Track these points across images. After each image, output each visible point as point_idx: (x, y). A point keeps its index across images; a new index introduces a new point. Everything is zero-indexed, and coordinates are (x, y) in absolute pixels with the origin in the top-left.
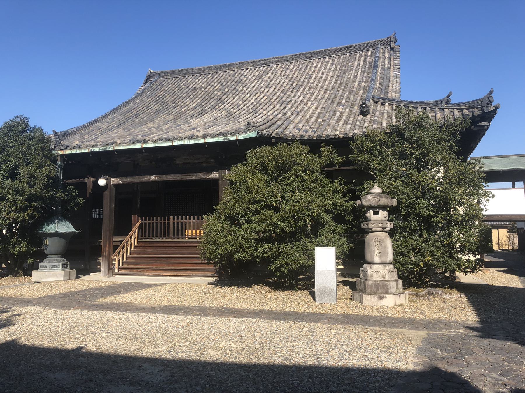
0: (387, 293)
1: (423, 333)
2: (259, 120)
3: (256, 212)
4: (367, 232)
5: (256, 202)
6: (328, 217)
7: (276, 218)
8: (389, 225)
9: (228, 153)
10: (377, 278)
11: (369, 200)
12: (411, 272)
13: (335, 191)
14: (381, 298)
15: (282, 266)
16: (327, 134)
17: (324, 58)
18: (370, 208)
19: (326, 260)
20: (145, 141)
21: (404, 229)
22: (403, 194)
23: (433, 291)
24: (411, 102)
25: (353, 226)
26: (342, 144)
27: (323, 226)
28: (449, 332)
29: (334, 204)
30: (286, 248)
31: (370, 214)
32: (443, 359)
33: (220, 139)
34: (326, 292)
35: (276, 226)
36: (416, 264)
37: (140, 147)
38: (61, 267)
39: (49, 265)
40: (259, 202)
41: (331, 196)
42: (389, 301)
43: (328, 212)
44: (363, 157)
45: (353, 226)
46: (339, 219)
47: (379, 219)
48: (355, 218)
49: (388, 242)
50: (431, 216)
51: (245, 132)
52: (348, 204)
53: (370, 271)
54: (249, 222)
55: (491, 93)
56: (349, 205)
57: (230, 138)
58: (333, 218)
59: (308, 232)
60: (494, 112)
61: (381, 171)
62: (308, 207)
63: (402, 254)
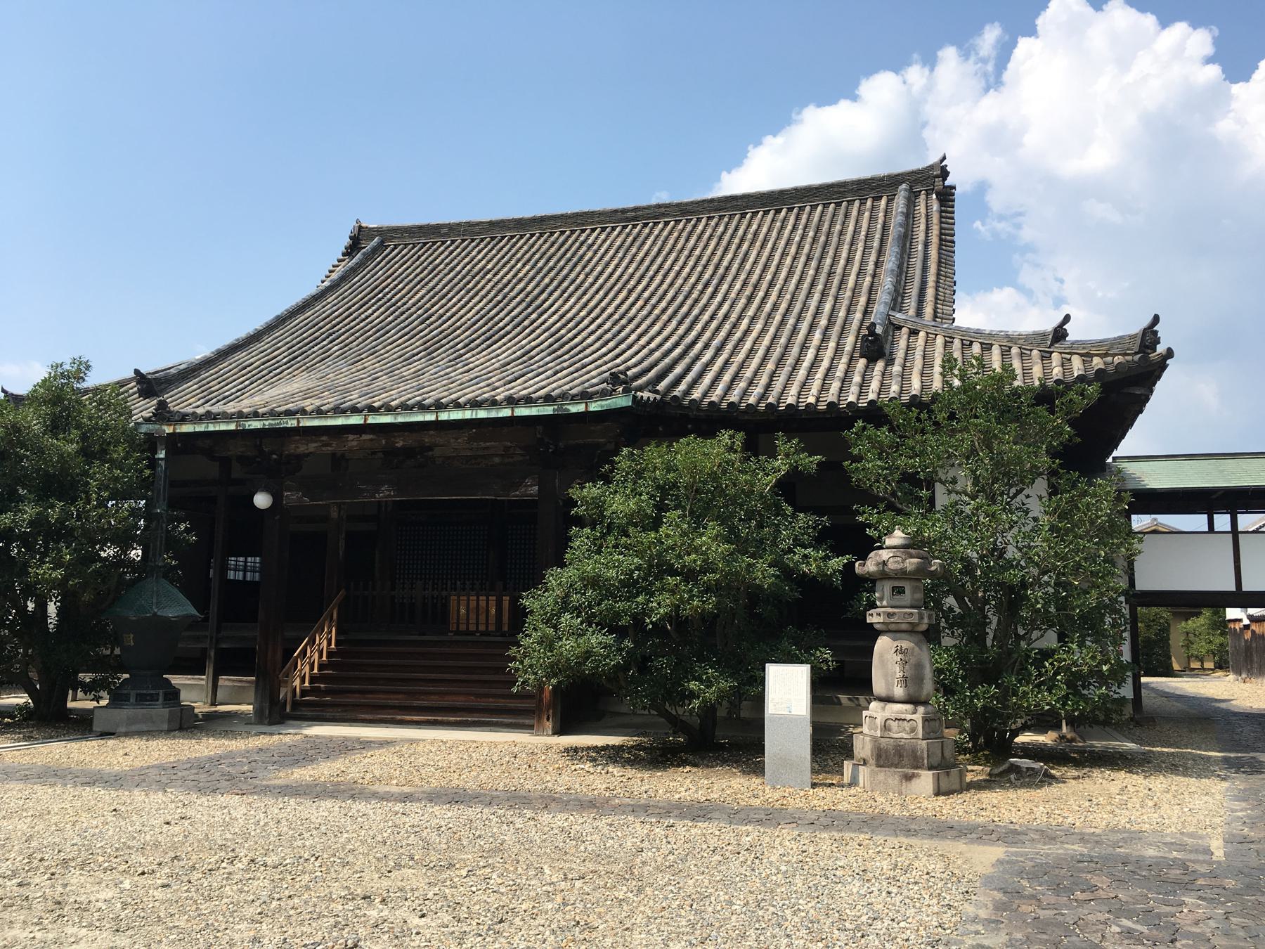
1: (996, 852)
2: (630, 362)
9: (566, 445)
16: (788, 402)
17: (778, 211)
19: (788, 689)
20: (372, 409)
24: (978, 332)
26: (823, 425)
28: (1055, 850)
32: (1033, 897)
33: (548, 410)
37: (362, 422)
38: (161, 699)
39: (133, 693)
51: (604, 394)
55: (1156, 319)
57: (569, 407)
60: (1161, 366)
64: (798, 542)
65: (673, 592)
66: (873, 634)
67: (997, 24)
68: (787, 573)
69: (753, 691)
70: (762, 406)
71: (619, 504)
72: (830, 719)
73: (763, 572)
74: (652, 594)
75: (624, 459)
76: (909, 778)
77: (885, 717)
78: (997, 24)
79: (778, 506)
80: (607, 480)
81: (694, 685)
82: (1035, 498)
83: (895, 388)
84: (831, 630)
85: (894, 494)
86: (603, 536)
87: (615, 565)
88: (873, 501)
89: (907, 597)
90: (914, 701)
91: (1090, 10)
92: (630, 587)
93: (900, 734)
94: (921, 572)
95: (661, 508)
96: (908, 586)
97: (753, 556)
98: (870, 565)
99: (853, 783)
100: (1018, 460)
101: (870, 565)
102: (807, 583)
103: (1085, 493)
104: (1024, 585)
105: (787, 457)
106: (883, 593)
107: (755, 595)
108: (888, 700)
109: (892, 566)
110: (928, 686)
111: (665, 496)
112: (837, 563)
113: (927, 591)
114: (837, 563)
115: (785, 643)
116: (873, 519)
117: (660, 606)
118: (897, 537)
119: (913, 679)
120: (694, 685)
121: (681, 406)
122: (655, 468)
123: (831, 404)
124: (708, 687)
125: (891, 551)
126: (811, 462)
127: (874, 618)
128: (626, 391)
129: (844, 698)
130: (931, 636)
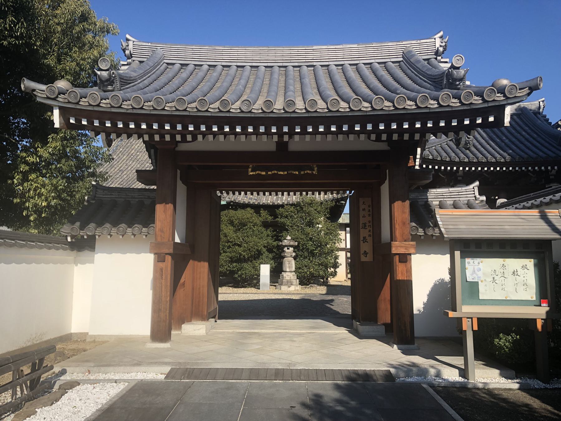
0: (292, 285)
3: (229, 247)
4: (284, 257)
5: (230, 242)
6: (264, 250)
7: (240, 250)
8: (294, 254)
10: (288, 278)
11: (285, 242)
12: (304, 278)
13: (268, 236)
14: (289, 287)
15: (242, 274)
18: (286, 246)
21: (301, 256)
22: (301, 239)
23: (313, 285)
25: (277, 254)
27: (262, 254)
29: (268, 243)
30: (245, 265)
31: (286, 249)
34: (265, 285)
35: (241, 255)
36: (306, 273)
40: (231, 242)
41: (264, 239)
42: (292, 288)
43: (265, 247)
44: (283, 220)
45: (277, 254)
46: (270, 251)
47: (289, 251)
48: (278, 250)
49: (293, 262)
50: (314, 250)
52: (275, 243)
53: (284, 275)
54: (224, 252)
56: (275, 243)
58: (267, 250)
59: (257, 256)
61: (292, 227)
62: (257, 246)
63: (300, 268)
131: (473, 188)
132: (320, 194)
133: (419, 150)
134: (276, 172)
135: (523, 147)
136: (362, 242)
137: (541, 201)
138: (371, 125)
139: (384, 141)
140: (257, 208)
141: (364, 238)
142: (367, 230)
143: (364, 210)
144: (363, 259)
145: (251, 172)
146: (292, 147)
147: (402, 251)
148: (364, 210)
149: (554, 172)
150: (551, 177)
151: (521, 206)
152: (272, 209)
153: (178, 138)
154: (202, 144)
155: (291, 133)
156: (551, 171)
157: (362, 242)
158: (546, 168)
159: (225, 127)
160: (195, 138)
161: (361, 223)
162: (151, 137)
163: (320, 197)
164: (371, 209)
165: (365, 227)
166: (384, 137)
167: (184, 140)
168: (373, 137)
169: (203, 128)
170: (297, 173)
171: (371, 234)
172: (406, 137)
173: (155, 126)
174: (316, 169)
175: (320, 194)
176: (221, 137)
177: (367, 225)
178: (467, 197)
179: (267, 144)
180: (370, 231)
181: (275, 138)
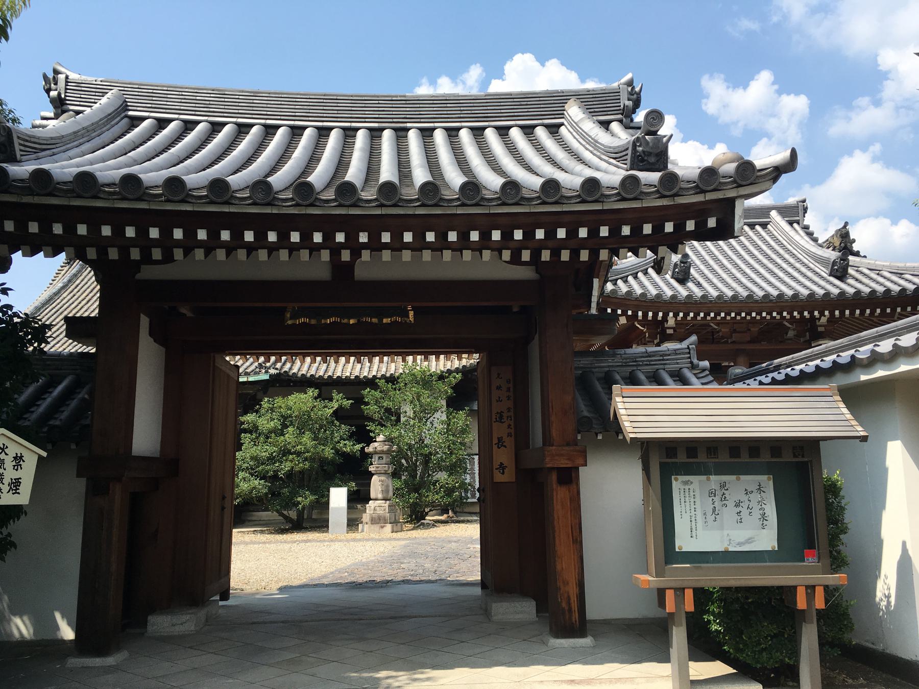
19: (338, 497)
51: (256, 373)
64: (342, 438)
65: (291, 461)
66: (371, 475)
67: (478, 65)
68: (337, 452)
69: (324, 500)
70: (326, 377)
71: (266, 423)
72: (354, 516)
73: (328, 452)
74: (282, 462)
75: (265, 403)
76: (382, 527)
77: (376, 506)
78: (478, 65)
79: (333, 422)
80: (257, 412)
81: (300, 499)
82: (441, 416)
83: (384, 369)
84: (354, 472)
85: (381, 418)
86: (257, 438)
87: (264, 450)
88: (373, 421)
89: (384, 461)
90: (385, 499)
91: (537, 64)
92: (271, 459)
93: (380, 512)
94: (388, 452)
95: (284, 426)
96: (384, 456)
97: (323, 445)
98: (369, 449)
99: (363, 531)
100: (428, 404)
101: (369, 449)
102: (344, 455)
103: (454, 417)
104: (430, 453)
105: (339, 400)
106: (375, 459)
107: (323, 461)
108: (376, 499)
109: (378, 449)
110: (391, 494)
111: (285, 421)
112: (358, 447)
113: (393, 457)
114: (358, 447)
115: (337, 481)
116: (373, 429)
117: (286, 466)
118: (381, 438)
119: (385, 491)
120: (300, 499)
121: (288, 375)
122: (280, 407)
123: (356, 377)
124: (305, 499)
125: (378, 445)
126: (347, 403)
127: (372, 469)
128: (267, 372)
129: (359, 506)
130: (395, 475)
131: (688, 348)
132: (437, 359)
133: (596, 282)
134: (343, 321)
135: (91, 295)
136: (495, 447)
137: (787, 375)
138: (543, 231)
139: (525, 264)
140: (325, 387)
141: (500, 439)
142: (505, 425)
143: (499, 388)
144: (499, 477)
145: (291, 319)
146: (360, 273)
147: (564, 463)
148: (499, 388)
149: (824, 320)
150: (820, 329)
151: (768, 380)
152: (354, 387)
153: (135, 254)
154: (220, 266)
155: (356, 250)
156: (819, 319)
157: (495, 447)
158: (811, 313)
159: (361, 234)
160: (168, 258)
161: (494, 411)
162: (102, 252)
163: (439, 364)
164: (511, 385)
165: (500, 418)
166: (526, 255)
167: (146, 258)
168: (506, 255)
169: (249, 236)
170: (375, 320)
171: (512, 431)
172: (584, 255)
173: (130, 232)
174: (411, 314)
175: (437, 359)
176: (284, 254)
177: (505, 415)
178: (678, 363)
179: (315, 267)
180: (509, 426)
181: (325, 255)
